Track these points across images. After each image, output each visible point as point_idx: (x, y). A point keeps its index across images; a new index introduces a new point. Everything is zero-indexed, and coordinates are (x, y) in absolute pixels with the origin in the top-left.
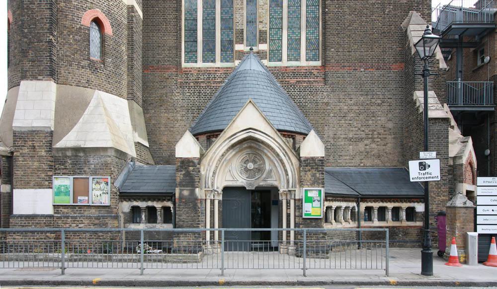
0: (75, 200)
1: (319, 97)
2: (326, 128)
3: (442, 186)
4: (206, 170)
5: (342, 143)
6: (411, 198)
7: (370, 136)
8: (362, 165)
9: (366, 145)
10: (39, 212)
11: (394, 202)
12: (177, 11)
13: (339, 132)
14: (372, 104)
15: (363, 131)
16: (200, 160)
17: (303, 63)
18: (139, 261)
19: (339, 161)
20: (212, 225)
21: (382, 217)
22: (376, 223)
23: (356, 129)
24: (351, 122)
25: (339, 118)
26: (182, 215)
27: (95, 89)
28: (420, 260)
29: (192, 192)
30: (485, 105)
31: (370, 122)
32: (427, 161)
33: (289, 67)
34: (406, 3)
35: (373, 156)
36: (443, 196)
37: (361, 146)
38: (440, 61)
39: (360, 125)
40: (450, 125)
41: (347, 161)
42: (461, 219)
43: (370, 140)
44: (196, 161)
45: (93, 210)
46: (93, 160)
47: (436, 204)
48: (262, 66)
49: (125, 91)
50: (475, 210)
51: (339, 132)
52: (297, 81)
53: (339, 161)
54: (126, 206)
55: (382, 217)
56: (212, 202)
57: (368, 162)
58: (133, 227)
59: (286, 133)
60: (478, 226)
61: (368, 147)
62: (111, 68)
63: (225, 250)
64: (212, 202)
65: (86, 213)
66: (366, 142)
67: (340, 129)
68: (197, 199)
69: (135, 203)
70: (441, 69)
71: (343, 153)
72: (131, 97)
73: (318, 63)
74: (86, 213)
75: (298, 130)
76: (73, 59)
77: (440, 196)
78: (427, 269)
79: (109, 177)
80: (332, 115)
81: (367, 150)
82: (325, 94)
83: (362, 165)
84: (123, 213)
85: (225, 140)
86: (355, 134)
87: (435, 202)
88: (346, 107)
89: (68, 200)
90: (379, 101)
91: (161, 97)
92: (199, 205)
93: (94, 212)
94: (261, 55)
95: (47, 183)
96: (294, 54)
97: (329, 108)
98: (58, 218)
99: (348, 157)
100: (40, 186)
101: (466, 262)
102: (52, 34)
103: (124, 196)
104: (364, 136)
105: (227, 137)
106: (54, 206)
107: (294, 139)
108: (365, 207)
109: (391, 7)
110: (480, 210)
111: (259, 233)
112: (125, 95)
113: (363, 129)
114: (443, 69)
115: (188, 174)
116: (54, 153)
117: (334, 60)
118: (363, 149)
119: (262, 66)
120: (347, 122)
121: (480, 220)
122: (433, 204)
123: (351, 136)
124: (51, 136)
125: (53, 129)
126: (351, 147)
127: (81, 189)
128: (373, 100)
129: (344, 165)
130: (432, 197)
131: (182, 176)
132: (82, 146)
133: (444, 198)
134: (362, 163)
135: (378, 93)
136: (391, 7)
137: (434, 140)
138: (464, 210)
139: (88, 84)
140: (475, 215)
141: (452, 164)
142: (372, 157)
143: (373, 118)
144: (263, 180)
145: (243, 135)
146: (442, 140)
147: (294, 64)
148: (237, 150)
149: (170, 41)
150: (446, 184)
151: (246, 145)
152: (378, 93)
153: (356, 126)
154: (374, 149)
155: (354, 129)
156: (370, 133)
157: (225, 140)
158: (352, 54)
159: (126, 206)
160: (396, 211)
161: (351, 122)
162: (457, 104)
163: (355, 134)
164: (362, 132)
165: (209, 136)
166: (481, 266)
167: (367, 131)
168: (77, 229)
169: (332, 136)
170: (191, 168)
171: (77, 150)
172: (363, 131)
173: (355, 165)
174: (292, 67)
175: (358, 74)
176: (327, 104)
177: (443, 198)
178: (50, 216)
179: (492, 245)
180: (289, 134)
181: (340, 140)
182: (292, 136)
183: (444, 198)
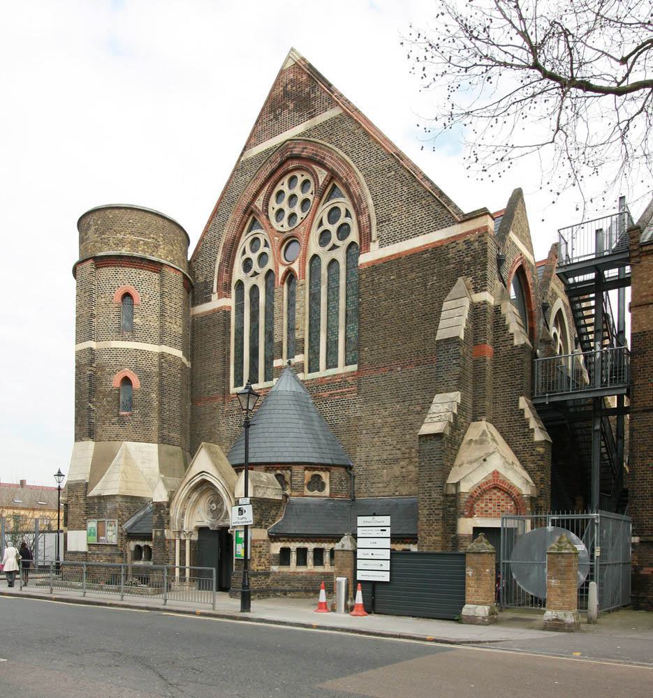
0: (98, 541)
1: (350, 412)
2: (358, 449)
3: (433, 522)
4: (175, 512)
5: (375, 467)
6: (404, 538)
7: (407, 455)
8: (397, 493)
9: (402, 468)
10: (80, 550)
11: (316, 541)
12: (224, 335)
13: (373, 453)
14: (409, 412)
15: (399, 449)
16: (169, 504)
17: (341, 369)
18: (82, 588)
19: (372, 490)
20: (182, 562)
21: (302, 560)
22: (310, 567)
23: (391, 447)
24: (385, 439)
25: (372, 436)
26: (156, 554)
27: (123, 441)
28: (240, 601)
29: (163, 533)
30: (571, 392)
31: (408, 436)
32: (243, 507)
33: (326, 377)
34: (453, 268)
35: (411, 481)
36: (435, 536)
37: (396, 470)
38: (515, 335)
39: (395, 443)
40: (528, 427)
41: (381, 490)
42: (339, 563)
43: (407, 460)
44: (165, 505)
45: (108, 548)
46: (109, 506)
47: (427, 546)
48: (297, 380)
49: (155, 435)
50: (355, 553)
51: (373, 453)
52: (330, 394)
53: (372, 490)
54: (132, 545)
55: (302, 560)
56: (183, 543)
57: (404, 490)
58: (137, 563)
59: (279, 466)
60: (358, 571)
61: (404, 470)
62: (139, 418)
63: (200, 589)
64: (183, 543)
65: (105, 551)
66: (402, 463)
67: (373, 449)
68: (165, 539)
69: (138, 543)
70: (516, 346)
71: (376, 480)
72: (163, 440)
73: (354, 368)
74: (105, 551)
75: (296, 460)
76: (106, 418)
77: (432, 536)
78: (246, 606)
79: (117, 521)
80: (364, 432)
81: (404, 474)
82: (357, 406)
83: (397, 493)
84: (131, 551)
85: (186, 485)
86: (390, 455)
87: (425, 543)
88: (380, 421)
89: (94, 540)
90: (418, 408)
91: (211, 429)
92: (167, 545)
93: (108, 550)
94: (300, 368)
95: (84, 526)
96: (331, 364)
97: (361, 423)
98: (90, 554)
99: (381, 485)
100: (80, 528)
101: (333, 610)
102: (90, 402)
103: (131, 536)
104: (400, 456)
105: (187, 481)
106: (88, 544)
107: (291, 470)
108: (281, 549)
109: (435, 278)
110: (360, 554)
111: (370, 586)
112: (156, 439)
113: (399, 446)
114: (519, 347)
115: (160, 517)
116: (88, 501)
117: (367, 363)
118: (398, 473)
119: (297, 380)
120: (381, 439)
121: (360, 565)
122: (423, 546)
123: (385, 457)
124: (87, 486)
125: (87, 481)
126: (385, 471)
127: (100, 532)
128: (411, 408)
129: (377, 494)
130: (421, 536)
131: (157, 518)
132: (102, 495)
133: (436, 538)
134: (397, 491)
135: (418, 397)
136: (435, 278)
137: (426, 463)
138: (341, 553)
139: (118, 438)
140: (355, 559)
141: (454, 493)
142: (410, 483)
143: (411, 431)
144: (222, 521)
145: (198, 479)
146: (434, 462)
147: (332, 371)
148: (200, 492)
149: (218, 368)
150: (439, 520)
151: (205, 488)
152: (418, 397)
153: (391, 443)
154: (411, 471)
155: (388, 448)
156: (407, 451)
157: (186, 485)
158: (388, 350)
159: (132, 545)
160: (302, 553)
161: (385, 439)
162: (555, 392)
163: (390, 455)
164: (398, 451)
165: (268, 468)
166: (348, 616)
167: (404, 449)
168: (97, 563)
169: (364, 458)
170: (162, 511)
171: (100, 497)
172: (399, 449)
173: (389, 494)
174: (329, 376)
175: (395, 375)
176: (359, 419)
177: (434, 538)
178: (86, 553)
179: (358, 592)
180: (283, 466)
181: (373, 462)
182: (289, 468)
183: (436, 538)
